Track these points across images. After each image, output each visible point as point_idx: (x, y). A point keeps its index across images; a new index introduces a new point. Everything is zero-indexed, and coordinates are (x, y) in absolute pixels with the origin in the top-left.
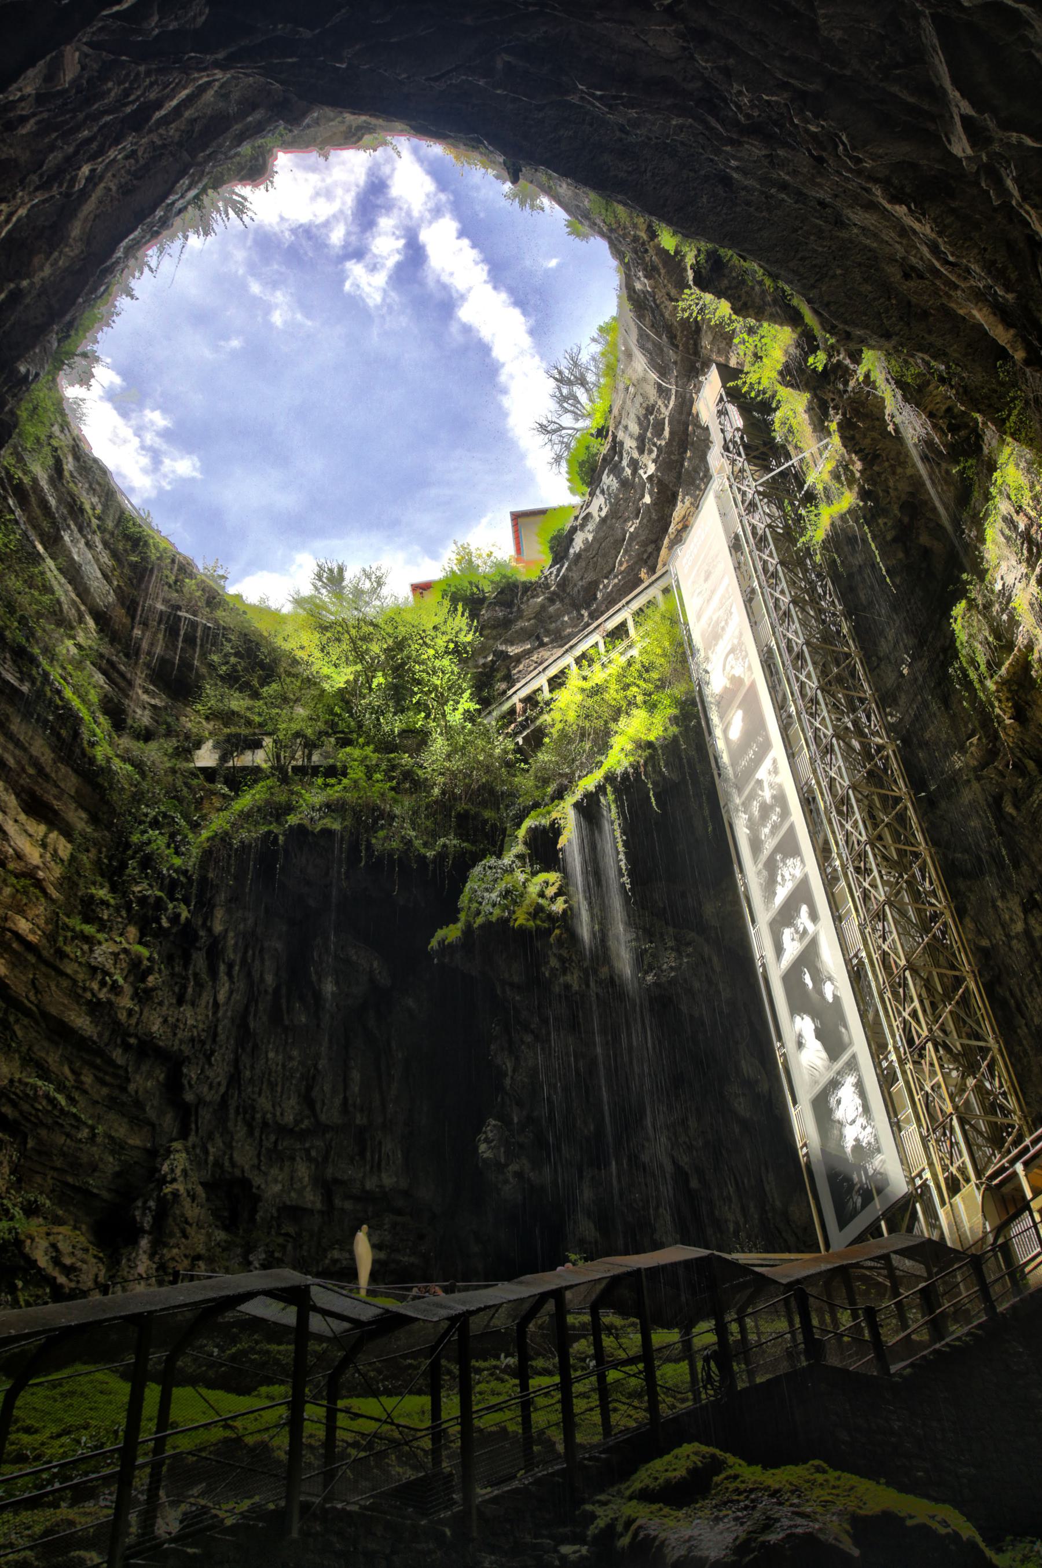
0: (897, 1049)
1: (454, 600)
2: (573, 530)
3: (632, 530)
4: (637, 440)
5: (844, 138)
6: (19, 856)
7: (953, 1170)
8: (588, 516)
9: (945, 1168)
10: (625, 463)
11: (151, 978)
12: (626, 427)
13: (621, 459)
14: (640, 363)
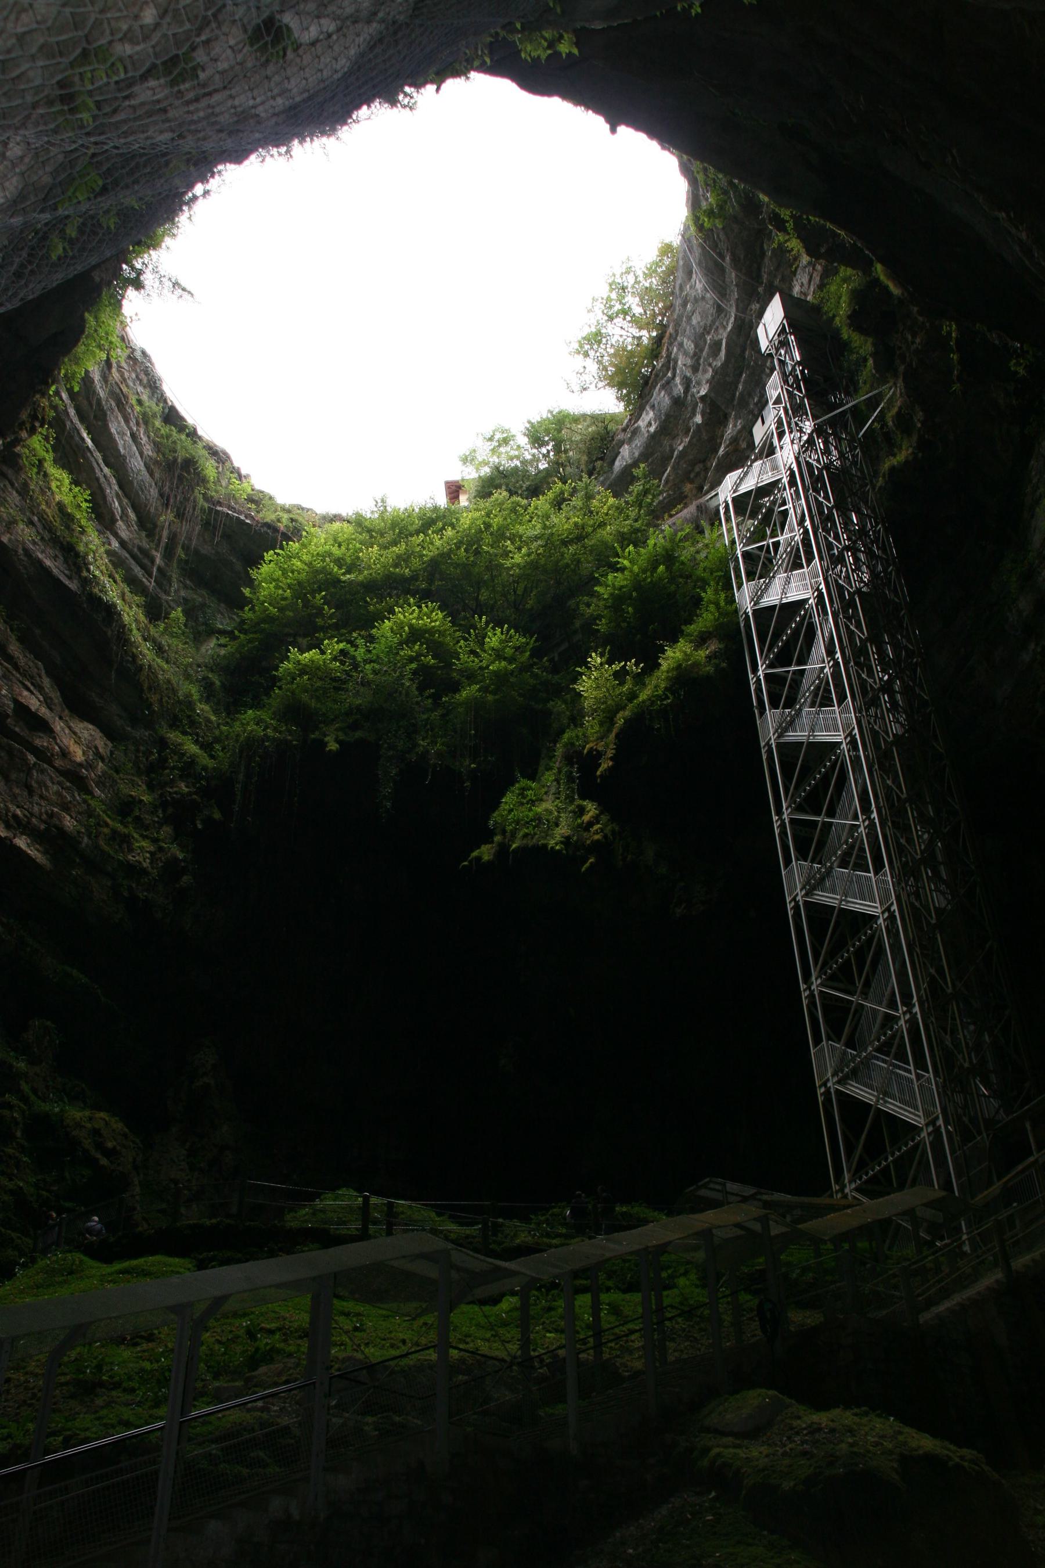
3: (681, 448)
4: (692, 358)
6: (65, 754)
8: (636, 432)
10: (678, 380)
11: (185, 878)
12: (681, 345)
13: (674, 376)
14: (699, 284)
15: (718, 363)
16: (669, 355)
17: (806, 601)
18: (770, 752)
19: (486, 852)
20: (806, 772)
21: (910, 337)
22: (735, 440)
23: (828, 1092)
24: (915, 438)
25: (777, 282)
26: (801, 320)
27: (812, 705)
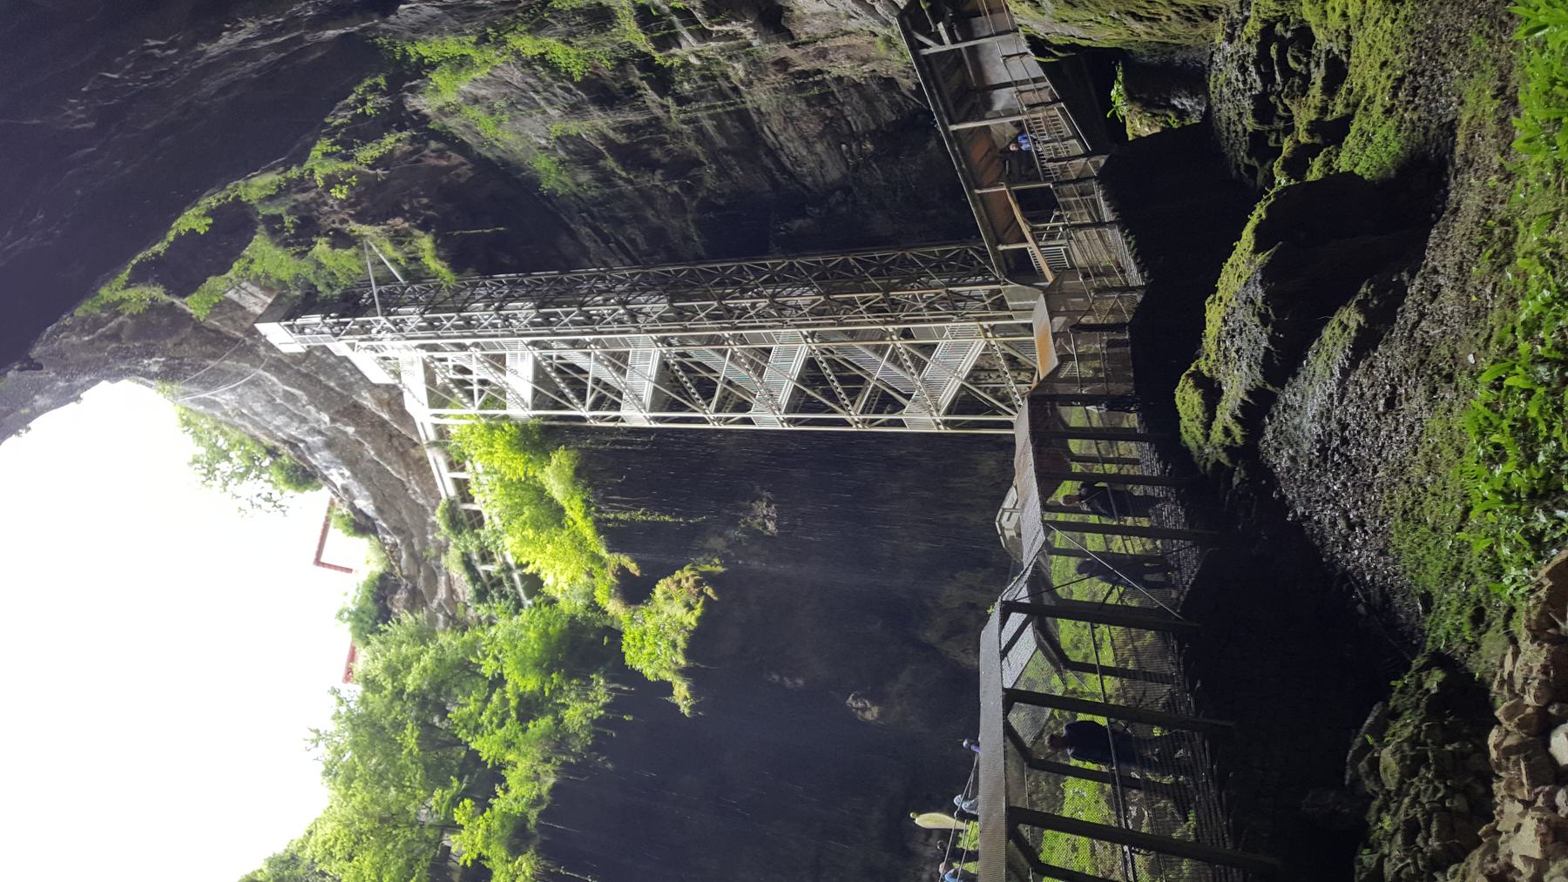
0: (887, 323)
1: (375, 630)
2: (352, 506)
5: (152, 43)
7: (988, 302)
8: (346, 490)
9: (985, 308)
10: (309, 439)
12: (278, 428)
14: (224, 396)
15: (304, 398)
16: (285, 442)
17: (535, 360)
18: (657, 419)
19: (681, 692)
20: (682, 391)
21: (326, 208)
22: (380, 402)
23: (946, 423)
24: (417, 232)
25: (246, 325)
26: (290, 309)
27: (624, 373)
